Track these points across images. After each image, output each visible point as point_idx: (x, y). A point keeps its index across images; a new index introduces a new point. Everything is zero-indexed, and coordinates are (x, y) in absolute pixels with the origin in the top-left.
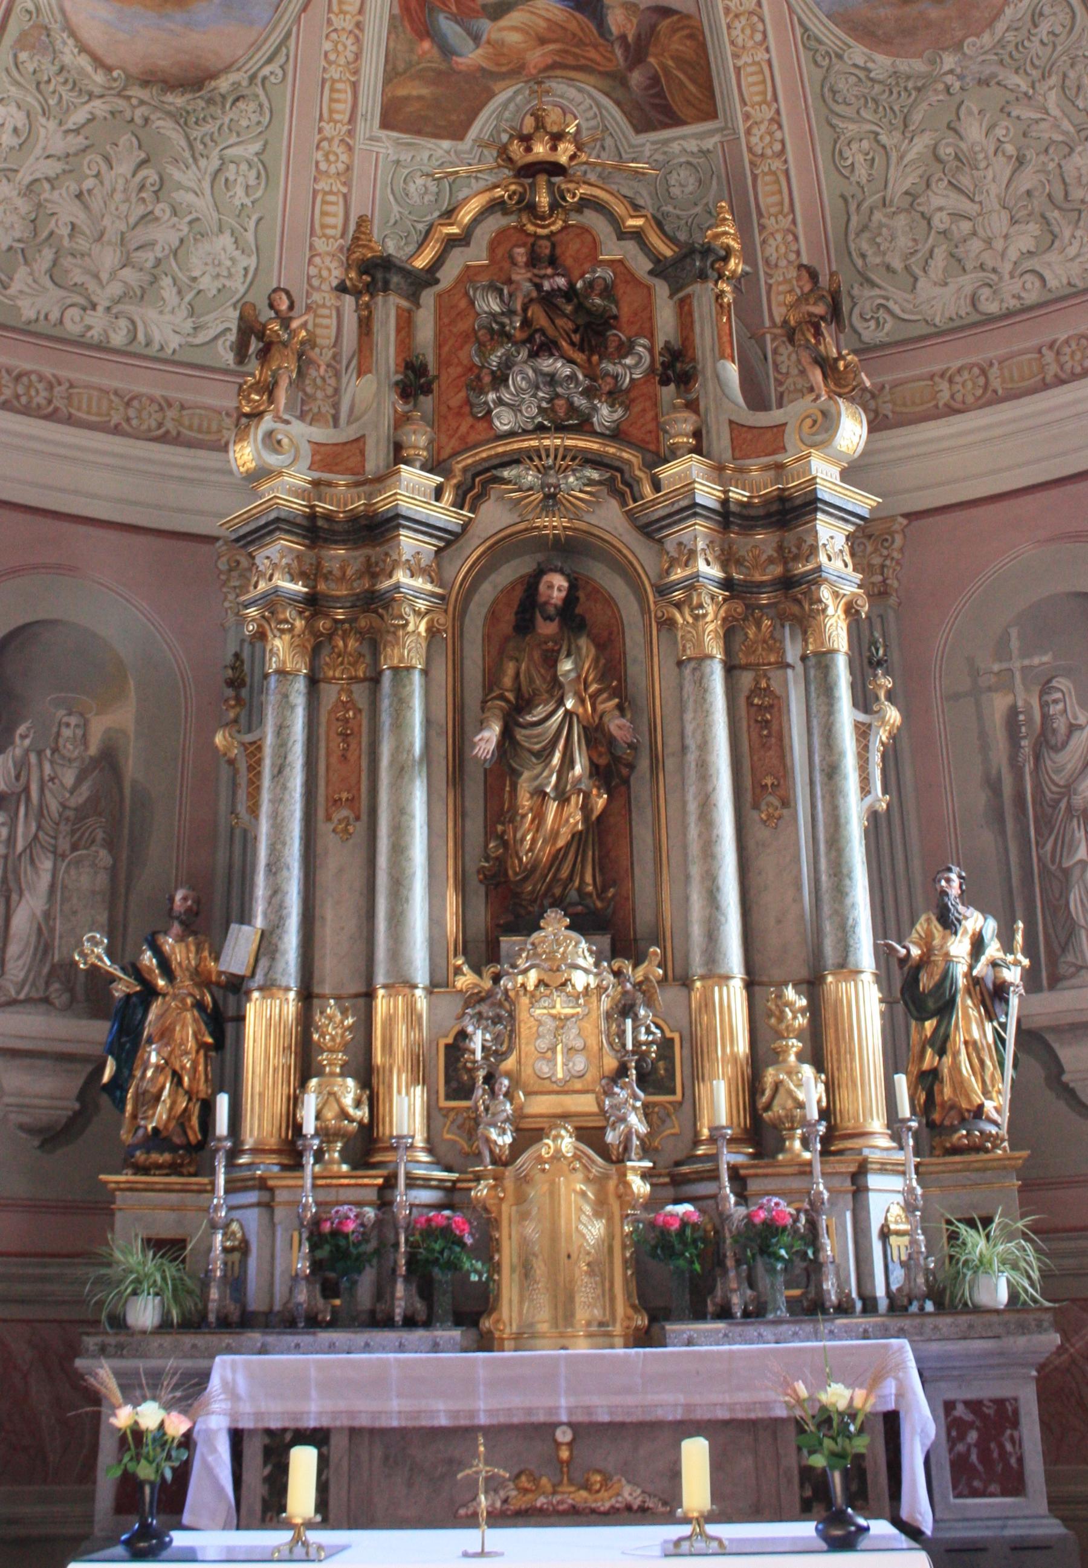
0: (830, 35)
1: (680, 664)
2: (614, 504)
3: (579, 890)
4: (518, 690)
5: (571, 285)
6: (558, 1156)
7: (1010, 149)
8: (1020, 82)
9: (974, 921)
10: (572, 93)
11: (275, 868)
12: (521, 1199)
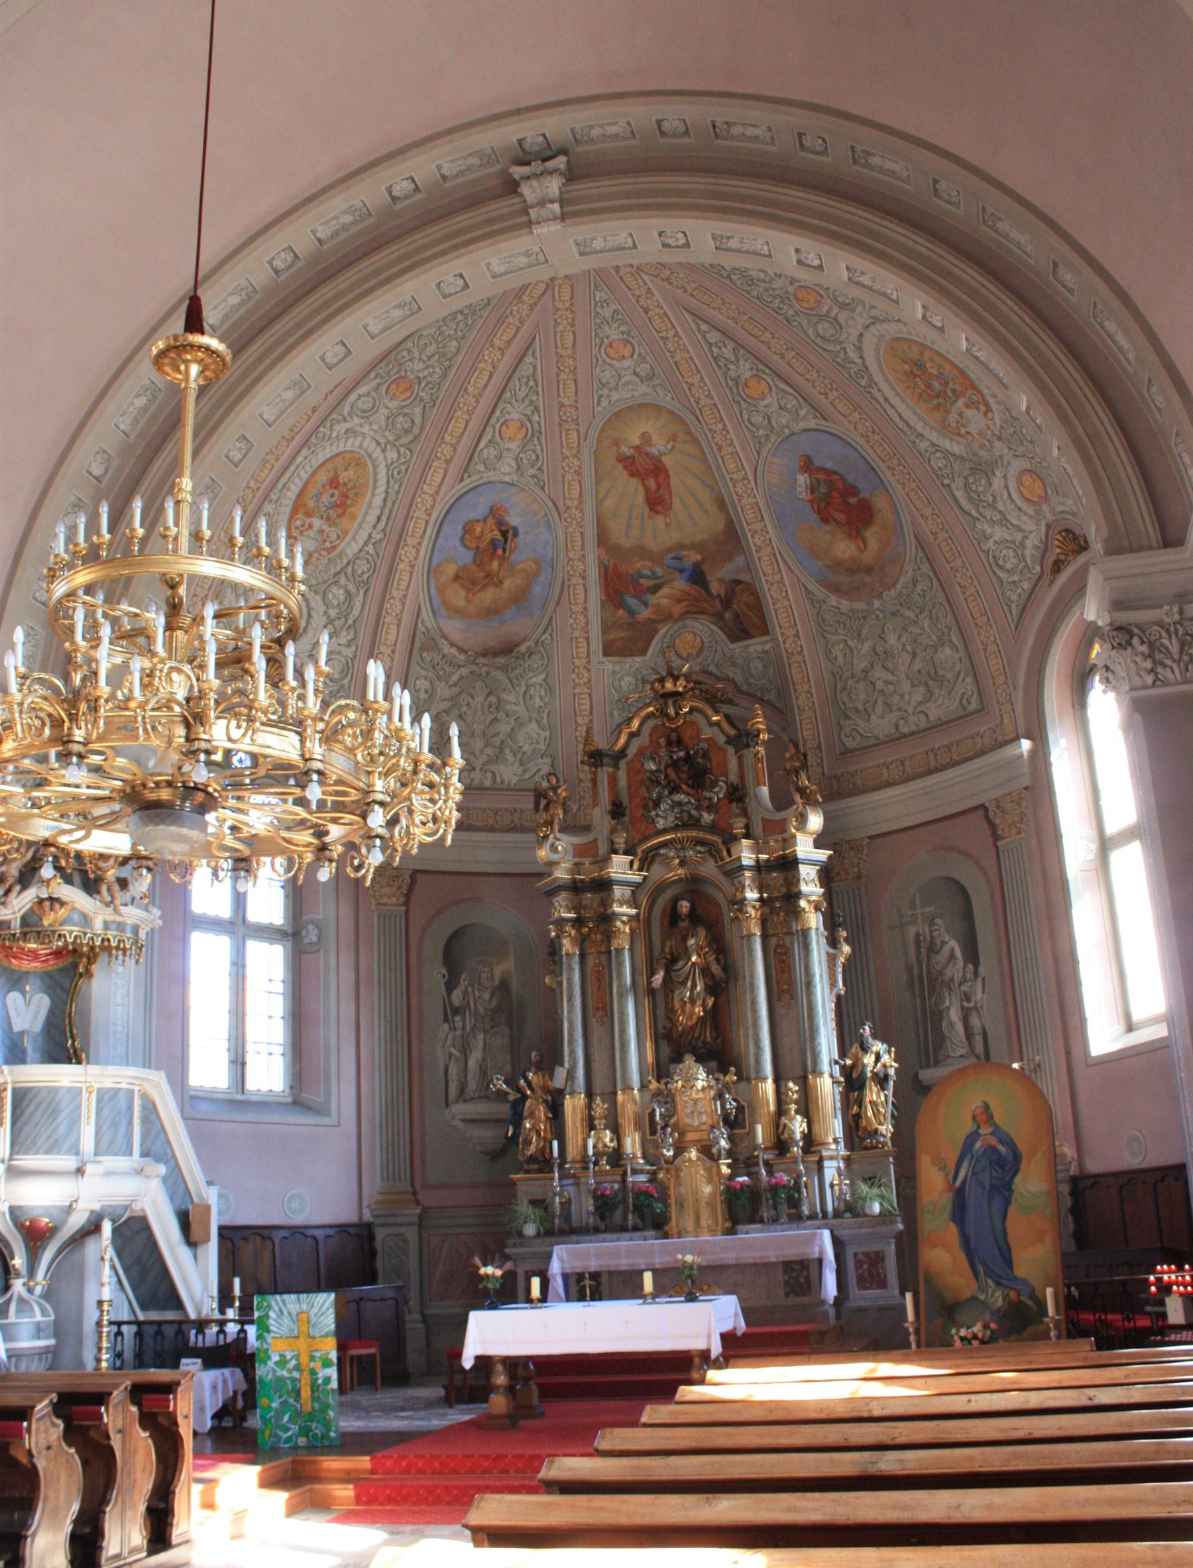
0: (820, 592)
1: (742, 937)
2: (712, 861)
3: (704, 1042)
4: (672, 954)
5: (688, 753)
6: (690, 1160)
7: (909, 648)
8: (910, 614)
9: (878, 1046)
10: (697, 625)
11: (571, 1041)
12: (677, 1176)
